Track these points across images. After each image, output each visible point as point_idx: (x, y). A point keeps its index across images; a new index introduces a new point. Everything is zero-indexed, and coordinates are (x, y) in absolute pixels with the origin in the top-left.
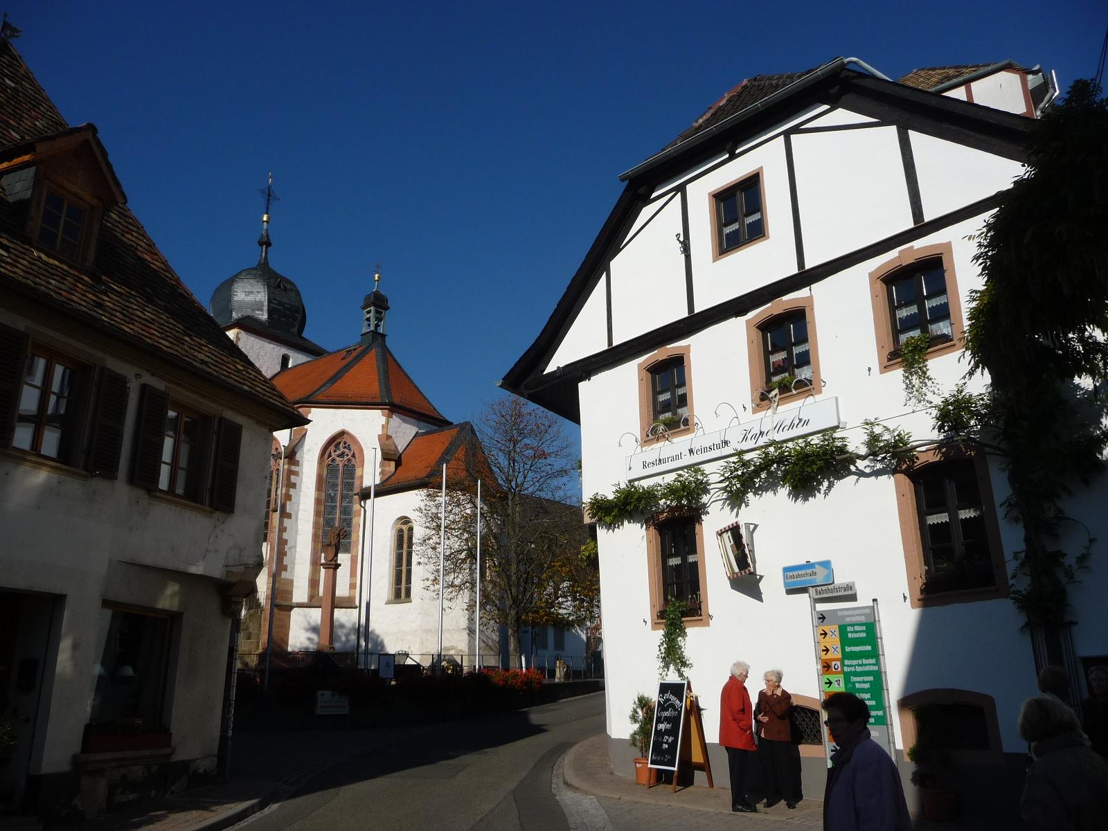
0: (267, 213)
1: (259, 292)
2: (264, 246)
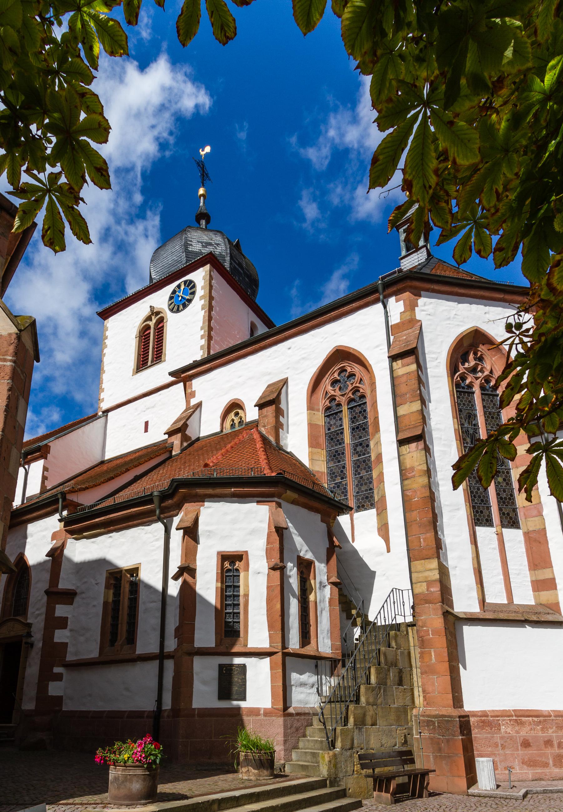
0: (203, 186)
1: (218, 244)
2: (203, 222)
